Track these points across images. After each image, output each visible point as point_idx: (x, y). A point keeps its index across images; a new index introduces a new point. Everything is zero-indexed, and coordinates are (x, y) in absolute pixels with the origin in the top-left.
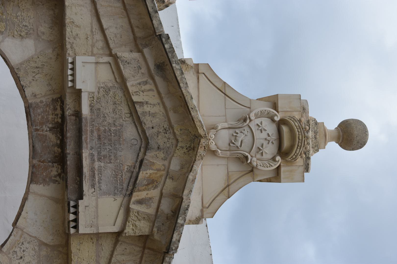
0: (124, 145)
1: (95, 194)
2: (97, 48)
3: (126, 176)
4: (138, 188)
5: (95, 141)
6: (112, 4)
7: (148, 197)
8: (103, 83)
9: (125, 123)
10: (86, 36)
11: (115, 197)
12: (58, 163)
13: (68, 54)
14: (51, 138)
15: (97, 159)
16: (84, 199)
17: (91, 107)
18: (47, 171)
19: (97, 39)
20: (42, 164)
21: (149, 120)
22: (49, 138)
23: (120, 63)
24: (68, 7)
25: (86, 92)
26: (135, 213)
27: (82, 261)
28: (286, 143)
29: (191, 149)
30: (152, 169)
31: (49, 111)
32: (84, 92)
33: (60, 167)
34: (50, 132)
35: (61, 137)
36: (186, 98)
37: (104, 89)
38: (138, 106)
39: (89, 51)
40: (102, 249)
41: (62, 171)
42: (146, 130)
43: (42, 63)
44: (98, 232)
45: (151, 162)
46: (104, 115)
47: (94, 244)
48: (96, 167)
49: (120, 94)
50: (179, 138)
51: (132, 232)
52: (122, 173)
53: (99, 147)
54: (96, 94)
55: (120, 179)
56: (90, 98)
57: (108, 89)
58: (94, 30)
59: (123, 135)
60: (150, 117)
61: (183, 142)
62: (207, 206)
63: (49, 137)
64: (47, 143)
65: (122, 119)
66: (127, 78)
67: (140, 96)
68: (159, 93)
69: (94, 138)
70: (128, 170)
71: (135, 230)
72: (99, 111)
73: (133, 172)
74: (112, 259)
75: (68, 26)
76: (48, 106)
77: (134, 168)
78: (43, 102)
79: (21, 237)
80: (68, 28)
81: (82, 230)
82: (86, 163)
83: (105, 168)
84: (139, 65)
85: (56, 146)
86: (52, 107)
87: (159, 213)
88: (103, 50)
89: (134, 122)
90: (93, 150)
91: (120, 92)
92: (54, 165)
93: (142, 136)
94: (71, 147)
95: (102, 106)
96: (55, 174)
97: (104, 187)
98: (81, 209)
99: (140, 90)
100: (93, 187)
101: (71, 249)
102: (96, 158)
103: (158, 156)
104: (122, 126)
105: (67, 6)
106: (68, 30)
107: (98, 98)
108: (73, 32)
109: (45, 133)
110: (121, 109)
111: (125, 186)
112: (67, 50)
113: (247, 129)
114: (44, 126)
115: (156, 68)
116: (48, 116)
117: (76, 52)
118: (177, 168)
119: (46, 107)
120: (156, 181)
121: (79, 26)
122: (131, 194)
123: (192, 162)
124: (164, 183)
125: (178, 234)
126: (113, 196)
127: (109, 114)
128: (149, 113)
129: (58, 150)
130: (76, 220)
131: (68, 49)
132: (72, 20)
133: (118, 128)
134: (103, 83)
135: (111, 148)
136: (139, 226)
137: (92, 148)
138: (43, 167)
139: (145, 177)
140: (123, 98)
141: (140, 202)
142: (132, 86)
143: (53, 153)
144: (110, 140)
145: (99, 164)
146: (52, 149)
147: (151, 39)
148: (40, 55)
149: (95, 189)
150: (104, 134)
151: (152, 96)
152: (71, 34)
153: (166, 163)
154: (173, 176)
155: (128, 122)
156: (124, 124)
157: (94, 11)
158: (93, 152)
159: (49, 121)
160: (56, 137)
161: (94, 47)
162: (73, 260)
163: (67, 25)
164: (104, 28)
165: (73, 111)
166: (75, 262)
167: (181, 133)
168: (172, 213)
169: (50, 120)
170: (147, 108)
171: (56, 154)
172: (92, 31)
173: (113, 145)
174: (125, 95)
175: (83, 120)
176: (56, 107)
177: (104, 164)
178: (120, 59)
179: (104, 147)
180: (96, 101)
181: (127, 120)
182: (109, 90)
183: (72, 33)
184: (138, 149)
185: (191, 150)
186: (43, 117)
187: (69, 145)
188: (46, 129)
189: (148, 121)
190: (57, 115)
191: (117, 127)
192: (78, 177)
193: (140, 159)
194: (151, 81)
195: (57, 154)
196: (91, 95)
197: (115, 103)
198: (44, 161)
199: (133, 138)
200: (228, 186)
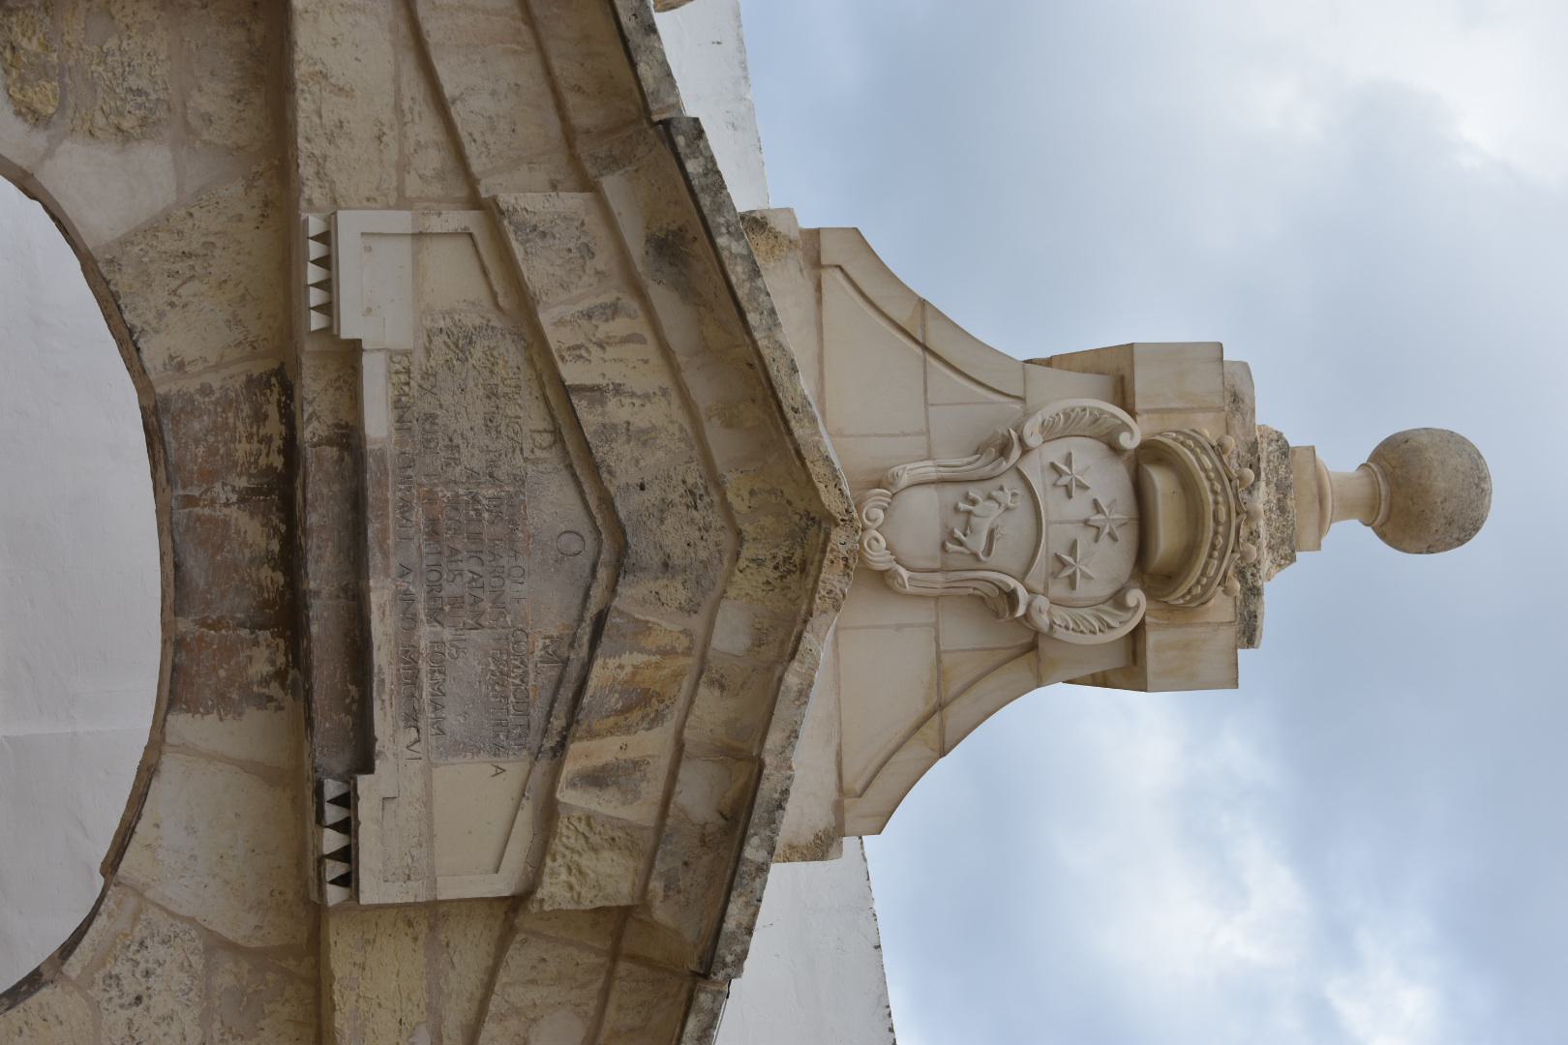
3: (540, 679)
8: (447, 316)
9: (534, 468)
10: (376, 129)
13: (304, 199)
14: (246, 532)
20: (213, 632)
22: (238, 532)
28: (1167, 539)
29: (794, 569)
30: (642, 651)
31: (235, 428)
32: (372, 351)
33: (282, 645)
34: (239, 508)
35: (283, 528)
36: (773, 371)
38: (584, 403)
40: (453, 963)
45: (637, 621)
47: (420, 943)
48: (424, 644)
49: (511, 355)
51: (568, 895)
53: (434, 568)
54: (419, 356)
57: (466, 337)
58: (406, 104)
61: (761, 540)
62: (858, 787)
65: (522, 453)
66: (537, 293)
68: (666, 351)
71: (577, 888)
73: (566, 662)
75: (303, 91)
76: (230, 405)
77: (571, 645)
78: (212, 392)
79: (136, 919)
80: (305, 99)
81: (372, 890)
82: (382, 629)
83: (457, 648)
84: (584, 240)
87: (669, 821)
89: (570, 466)
90: (410, 578)
91: (512, 349)
94: (323, 566)
95: (441, 406)
97: (453, 721)
100: (412, 723)
102: (421, 609)
105: (298, 13)
106: (305, 105)
107: (426, 375)
109: (221, 513)
111: (537, 715)
112: (303, 184)
113: (1010, 483)
119: (224, 411)
121: (347, 88)
123: (799, 620)
124: (691, 702)
127: (470, 434)
128: (628, 430)
130: (347, 854)
131: (305, 181)
135: (478, 569)
136: (593, 871)
137: (405, 571)
138: (215, 647)
141: (596, 779)
142: (561, 323)
144: (475, 537)
149: (418, 731)
151: (638, 360)
152: (318, 121)
153: (696, 623)
154: (722, 676)
155: (545, 465)
157: (404, 29)
159: (235, 464)
160: (263, 526)
162: (337, 1008)
163: (300, 86)
165: (329, 427)
169: (241, 462)
170: (618, 411)
171: (266, 595)
172: (398, 109)
179: (453, 566)
180: (420, 386)
183: (321, 117)
184: (588, 570)
186: (212, 451)
188: (224, 497)
189: (623, 463)
190: (267, 440)
193: (593, 609)
194: (632, 304)
195: (268, 592)
196: (401, 364)
197: (492, 394)
198: (219, 621)
200: (940, 707)
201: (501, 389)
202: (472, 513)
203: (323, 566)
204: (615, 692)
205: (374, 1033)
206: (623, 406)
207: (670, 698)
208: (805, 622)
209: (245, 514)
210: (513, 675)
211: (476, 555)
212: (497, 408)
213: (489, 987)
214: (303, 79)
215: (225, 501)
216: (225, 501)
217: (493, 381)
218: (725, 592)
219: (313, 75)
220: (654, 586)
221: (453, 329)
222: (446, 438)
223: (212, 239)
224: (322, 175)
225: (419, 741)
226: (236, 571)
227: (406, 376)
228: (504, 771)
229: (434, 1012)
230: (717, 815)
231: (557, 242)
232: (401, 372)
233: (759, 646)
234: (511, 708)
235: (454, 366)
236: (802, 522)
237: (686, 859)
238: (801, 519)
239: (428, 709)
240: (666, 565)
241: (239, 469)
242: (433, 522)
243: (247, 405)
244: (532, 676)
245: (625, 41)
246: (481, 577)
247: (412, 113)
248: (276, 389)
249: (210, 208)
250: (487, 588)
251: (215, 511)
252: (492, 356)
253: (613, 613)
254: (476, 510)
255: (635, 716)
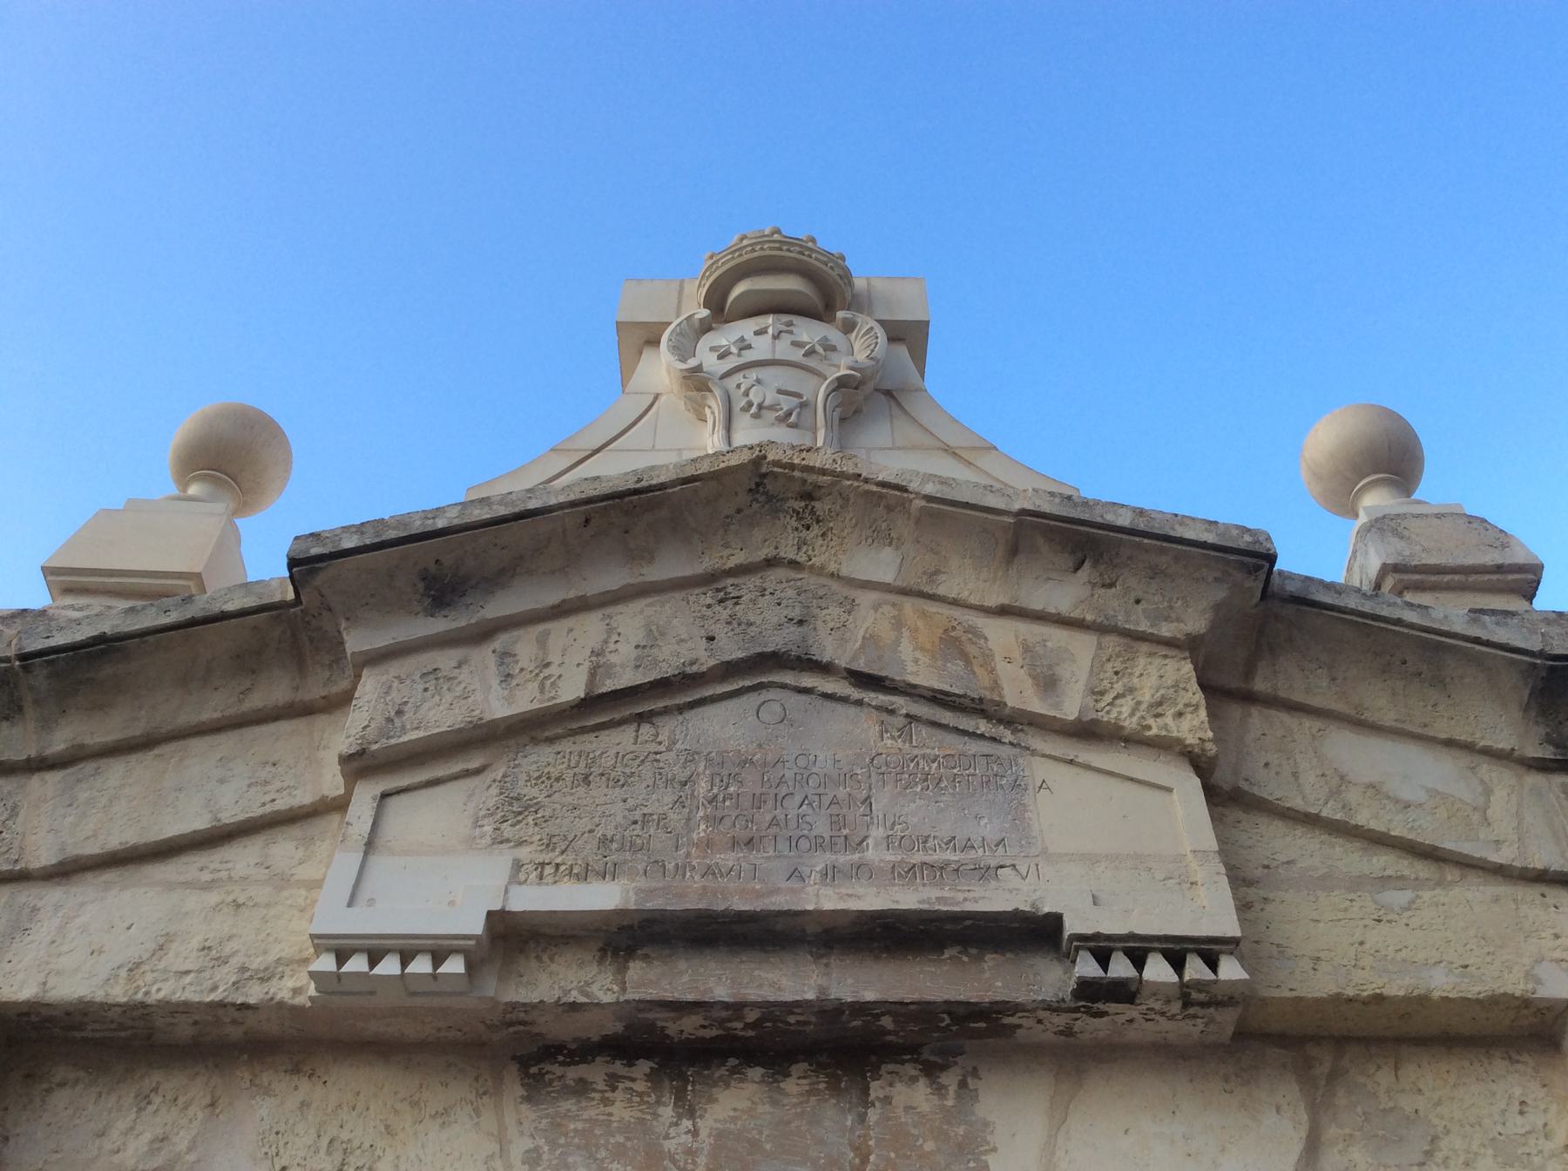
0: (783, 749)
1: (1026, 866)
2: (300, 864)
3: (929, 742)
4: (983, 691)
5: (758, 862)
6: (103, 795)
7: (1021, 659)
8: (479, 823)
9: (680, 742)
10: (225, 910)
11: (1031, 787)
12: (869, 1074)
13: (293, 998)
14: (735, 1110)
15: (854, 853)
16: (1062, 912)
17: (584, 875)
18: (914, 1131)
19: (252, 864)
20: (872, 1158)
21: (676, 647)
22: (734, 1119)
23: (393, 742)
24: (47, 987)
25: (506, 891)
26: (1102, 704)
27: (1372, 952)
29: (810, 507)
30: (897, 642)
31: (589, 1120)
32: (505, 899)
33: (891, 1067)
34: (701, 1117)
35: (732, 1061)
37: (507, 820)
38: (608, 682)
39: (306, 898)
40: (1288, 863)
41: (908, 1057)
42: (718, 659)
43: (317, 1152)
44: (1215, 852)
45: (863, 646)
46: (635, 822)
47: (1271, 896)
48: (891, 857)
49: (539, 758)
50: (759, 553)
51: (1189, 716)
52: (916, 757)
53: (793, 844)
55: (946, 768)
56: (544, 881)
57: (511, 804)
58: (206, 876)
59: (740, 751)
60: (661, 644)
61: (777, 542)
63: (725, 1121)
64: (760, 1133)
65: (661, 753)
66: (469, 719)
67: (560, 676)
68: (561, 611)
69: (747, 866)
70: (899, 737)
71: (1180, 706)
72: (612, 841)
74: (1330, 816)
75: (147, 993)
76: (559, 1125)
77: (892, 712)
78: (537, 1149)
80: (159, 990)
83: (894, 824)
84: (417, 677)
85: (779, 1087)
86: (568, 1105)
87: (1089, 617)
88: (316, 838)
89: (680, 709)
90: (805, 870)
91: (533, 758)
92: (882, 1096)
93: (748, 683)
94: (784, 982)
95: (591, 831)
96: (929, 1090)
97: (989, 828)
98: (1111, 924)
99: (537, 675)
100: (992, 872)
101: (1325, 996)
102: (844, 859)
103: (838, 625)
104: (691, 756)
105: (41, 995)
107: (549, 846)
108: (186, 969)
110: (617, 757)
111: (975, 747)
112: (272, 999)
113: (731, 383)
114: (669, 1145)
115: (443, 613)
116: (615, 1125)
117: (297, 958)
118: (888, 554)
119: (566, 1135)
120: (946, 630)
121: (161, 940)
122: (1018, 721)
123: (867, 487)
124: (955, 603)
125: (1181, 524)
126: (1030, 791)
127: (631, 802)
128: (644, 647)
129: (799, 1078)
131: (269, 996)
132: (123, 973)
133: (701, 769)
134: (479, 823)
135: (798, 798)
136: (1157, 691)
137: (795, 874)
138: (893, 1155)
139: (932, 667)
140: (566, 746)
143: (813, 1098)
144: (758, 801)
145: (876, 845)
146: (795, 1105)
147: (311, 640)
148: (276, 1159)
149: (1002, 867)
150: (728, 822)
151: (567, 637)
152: (192, 975)
154: (924, 573)
155: (678, 732)
156: (688, 748)
157: (110, 875)
158: (818, 869)
159: (642, 1121)
160: (728, 1086)
161: (292, 875)
162: (1378, 991)
163: (140, 996)
164: (209, 829)
165: (600, 973)
166: (1386, 980)
167: (739, 547)
168: (1087, 565)
169: (639, 1114)
171: (822, 1086)
173: (783, 790)
174: (551, 740)
175: (649, 905)
176: (572, 1083)
177: (875, 826)
178: (370, 743)
179: (792, 824)
180: (563, 852)
181: (667, 734)
182: (518, 799)
183: (188, 972)
184: (803, 698)
185: (813, 507)
187: (779, 989)
188: (684, 1137)
191: (698, 775)
192: (943, 954)
194: (499, 642)
195: (818, 1083)
198: (856, 1149)
199: (755, 717)
201: (581, 769)
202: (727, 803)
203: (784, 982)
204: (945, 666)
205: (1400, 950)
206: (617, 650)
207: (950, 621)
208: (866, 481)
209: (709, 1110)
210: (927, 769)
211: (779, 801)
212: (603, 775)
213: (1310, 820)
214: (131, 992)
215: (689, 1136)
216: (689, 1136)
217: (569, 780)
218: (832, 575)
219: (130, 979)
220: (823, 632)
221: (499, 816)
222: (634, 826)
223: (325, 1141)
224: (267, 974)
225: (1014, 866)
226: (789, 1123)
227: (547, 867)
228: (1044, 781)
229: (1357, 884)
230: (1080, 572)
231: (412, 700)
232: (542, 872)
233: (892, 539)
234: (967, 772)
235: (543, 817)
236: (760, 500)
237: (1132, 601)
238: (758, 502)
239: (972, 854)
240: (801, 623)
241: (649, 1117)
242: (734, 844)
243: (562, 1104)
244: (928, 751)
245: (193, 623)
246: (806, 797)
247: (219, 871)
248: (547, 1067)
249: (281, 1143)
250: (821, 790)
251: (703, 1148)
252: (540, 777)
253: (855, 667)
254: (724, 801)
255: (972, 650)
